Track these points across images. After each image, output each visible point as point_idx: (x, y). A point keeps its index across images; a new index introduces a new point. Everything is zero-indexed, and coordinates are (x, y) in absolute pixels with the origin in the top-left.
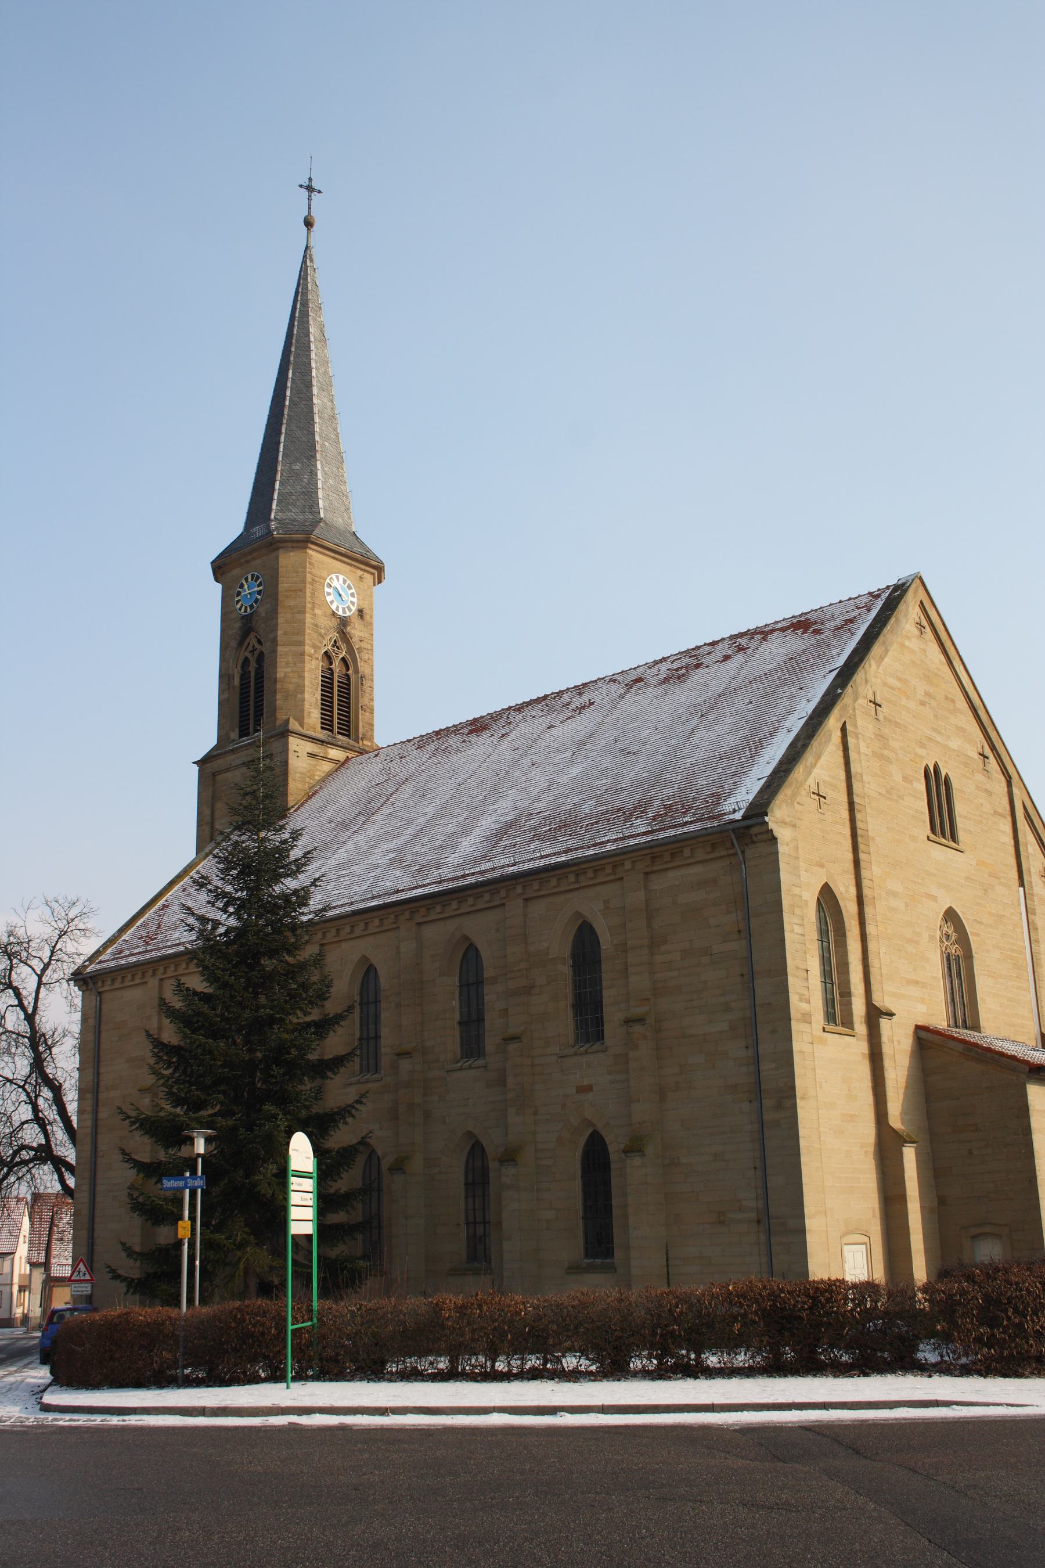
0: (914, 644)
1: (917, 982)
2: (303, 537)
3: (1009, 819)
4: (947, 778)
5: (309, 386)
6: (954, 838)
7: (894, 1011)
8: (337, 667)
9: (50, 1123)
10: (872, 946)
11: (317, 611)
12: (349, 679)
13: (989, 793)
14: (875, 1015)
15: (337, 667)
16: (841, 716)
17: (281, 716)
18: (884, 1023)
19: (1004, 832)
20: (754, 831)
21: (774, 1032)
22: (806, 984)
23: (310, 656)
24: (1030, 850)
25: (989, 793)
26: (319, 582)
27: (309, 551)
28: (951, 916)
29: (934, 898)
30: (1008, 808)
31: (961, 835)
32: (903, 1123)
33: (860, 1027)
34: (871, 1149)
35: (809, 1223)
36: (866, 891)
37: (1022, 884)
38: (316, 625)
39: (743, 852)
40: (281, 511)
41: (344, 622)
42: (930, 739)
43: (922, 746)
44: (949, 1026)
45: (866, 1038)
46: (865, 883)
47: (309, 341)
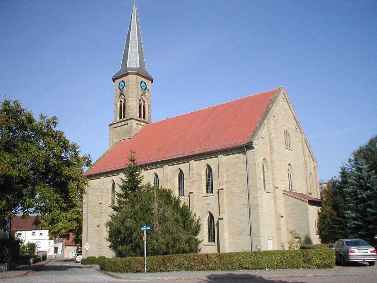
0: (282, 103)
9: (183, 223)
13: (297, 137)
20: (249, 146)
25: (297, 137)
42: (285, 124)
44: (290, 190)
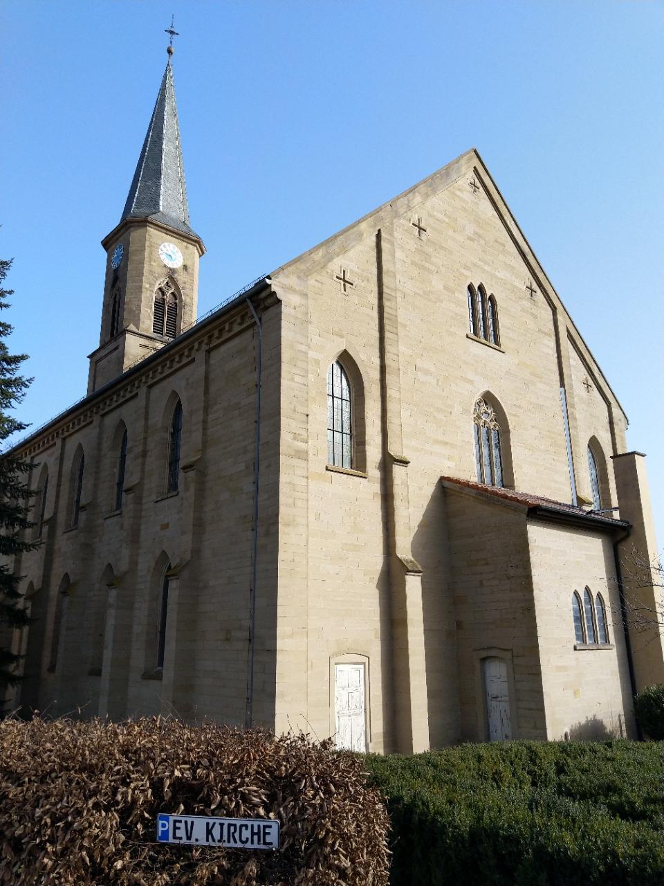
0: (466, 194)
1: (446, 443)
2: (144, 222)
3: (554, 338)
4: (492, 299)
5: (161, 139)
6: (497, 342)
7: (409, 459)
8: (168, 296)
10: (391, 406)
11: (152, 263)
12: (176, 305)
14: (388, 462)
15: (168, 296)
16: (375, 225)
17: (125, 324)
18: (397, 470)
19: (548, 347)
21: (269, 466)
22: (304, 426)
23: (146, 289)
24: (572, 362)
26: (155, 247)
27: (148, 228)
28: (489, 399)
29: (471, 382)
30: (553, 328)
31: (502, 340)
32: (413, 556)
33: (374, 472)
34: (377, 576)
35: (280, 644)
36: (388, 362)
37: (562, 385)
38: (151, 271)
39: (260, 319)
40: (137, 208)
41: (173, 271)
43: (466, 267)
45: (379, 480)
46: (388, 356)
47: (164, 115)
